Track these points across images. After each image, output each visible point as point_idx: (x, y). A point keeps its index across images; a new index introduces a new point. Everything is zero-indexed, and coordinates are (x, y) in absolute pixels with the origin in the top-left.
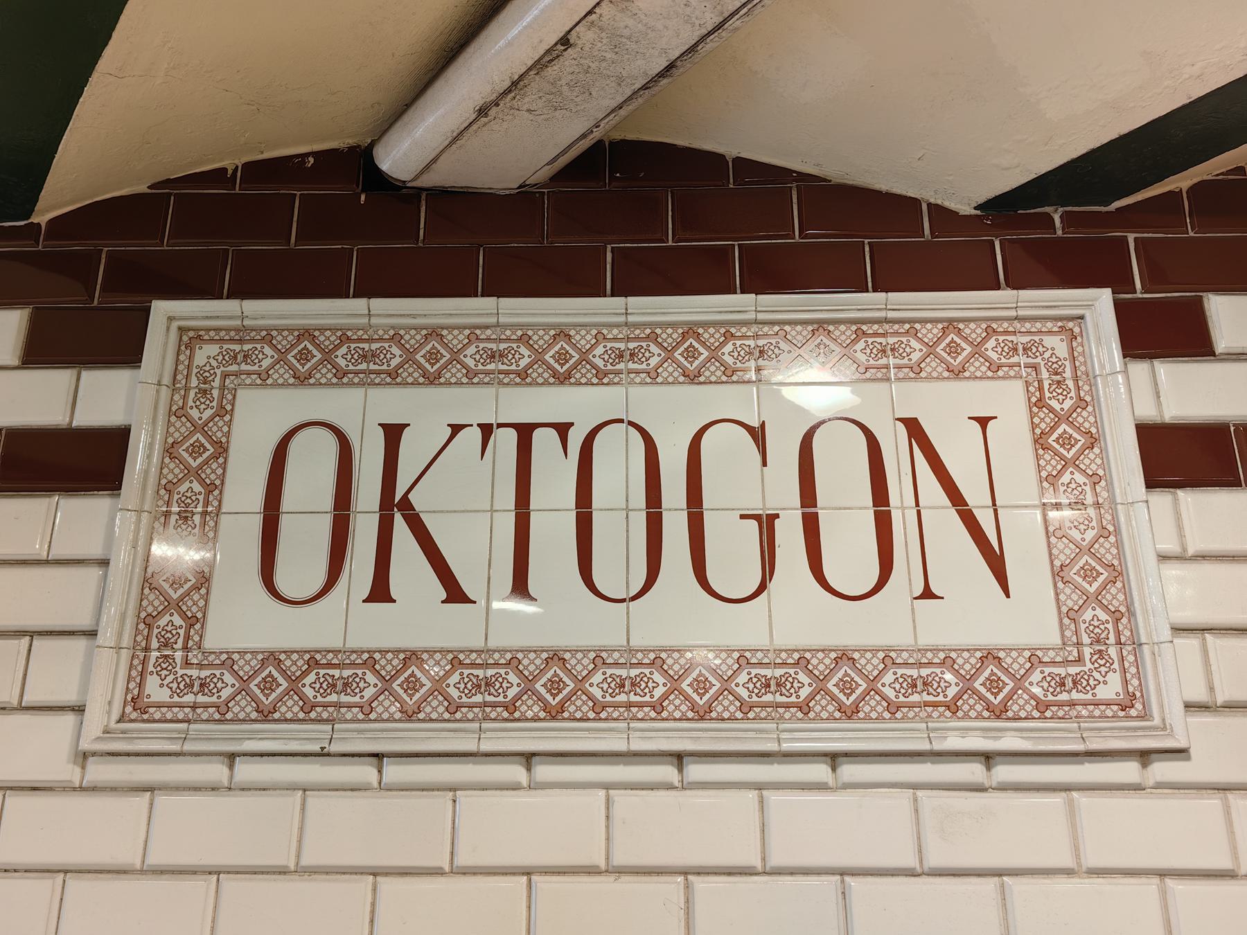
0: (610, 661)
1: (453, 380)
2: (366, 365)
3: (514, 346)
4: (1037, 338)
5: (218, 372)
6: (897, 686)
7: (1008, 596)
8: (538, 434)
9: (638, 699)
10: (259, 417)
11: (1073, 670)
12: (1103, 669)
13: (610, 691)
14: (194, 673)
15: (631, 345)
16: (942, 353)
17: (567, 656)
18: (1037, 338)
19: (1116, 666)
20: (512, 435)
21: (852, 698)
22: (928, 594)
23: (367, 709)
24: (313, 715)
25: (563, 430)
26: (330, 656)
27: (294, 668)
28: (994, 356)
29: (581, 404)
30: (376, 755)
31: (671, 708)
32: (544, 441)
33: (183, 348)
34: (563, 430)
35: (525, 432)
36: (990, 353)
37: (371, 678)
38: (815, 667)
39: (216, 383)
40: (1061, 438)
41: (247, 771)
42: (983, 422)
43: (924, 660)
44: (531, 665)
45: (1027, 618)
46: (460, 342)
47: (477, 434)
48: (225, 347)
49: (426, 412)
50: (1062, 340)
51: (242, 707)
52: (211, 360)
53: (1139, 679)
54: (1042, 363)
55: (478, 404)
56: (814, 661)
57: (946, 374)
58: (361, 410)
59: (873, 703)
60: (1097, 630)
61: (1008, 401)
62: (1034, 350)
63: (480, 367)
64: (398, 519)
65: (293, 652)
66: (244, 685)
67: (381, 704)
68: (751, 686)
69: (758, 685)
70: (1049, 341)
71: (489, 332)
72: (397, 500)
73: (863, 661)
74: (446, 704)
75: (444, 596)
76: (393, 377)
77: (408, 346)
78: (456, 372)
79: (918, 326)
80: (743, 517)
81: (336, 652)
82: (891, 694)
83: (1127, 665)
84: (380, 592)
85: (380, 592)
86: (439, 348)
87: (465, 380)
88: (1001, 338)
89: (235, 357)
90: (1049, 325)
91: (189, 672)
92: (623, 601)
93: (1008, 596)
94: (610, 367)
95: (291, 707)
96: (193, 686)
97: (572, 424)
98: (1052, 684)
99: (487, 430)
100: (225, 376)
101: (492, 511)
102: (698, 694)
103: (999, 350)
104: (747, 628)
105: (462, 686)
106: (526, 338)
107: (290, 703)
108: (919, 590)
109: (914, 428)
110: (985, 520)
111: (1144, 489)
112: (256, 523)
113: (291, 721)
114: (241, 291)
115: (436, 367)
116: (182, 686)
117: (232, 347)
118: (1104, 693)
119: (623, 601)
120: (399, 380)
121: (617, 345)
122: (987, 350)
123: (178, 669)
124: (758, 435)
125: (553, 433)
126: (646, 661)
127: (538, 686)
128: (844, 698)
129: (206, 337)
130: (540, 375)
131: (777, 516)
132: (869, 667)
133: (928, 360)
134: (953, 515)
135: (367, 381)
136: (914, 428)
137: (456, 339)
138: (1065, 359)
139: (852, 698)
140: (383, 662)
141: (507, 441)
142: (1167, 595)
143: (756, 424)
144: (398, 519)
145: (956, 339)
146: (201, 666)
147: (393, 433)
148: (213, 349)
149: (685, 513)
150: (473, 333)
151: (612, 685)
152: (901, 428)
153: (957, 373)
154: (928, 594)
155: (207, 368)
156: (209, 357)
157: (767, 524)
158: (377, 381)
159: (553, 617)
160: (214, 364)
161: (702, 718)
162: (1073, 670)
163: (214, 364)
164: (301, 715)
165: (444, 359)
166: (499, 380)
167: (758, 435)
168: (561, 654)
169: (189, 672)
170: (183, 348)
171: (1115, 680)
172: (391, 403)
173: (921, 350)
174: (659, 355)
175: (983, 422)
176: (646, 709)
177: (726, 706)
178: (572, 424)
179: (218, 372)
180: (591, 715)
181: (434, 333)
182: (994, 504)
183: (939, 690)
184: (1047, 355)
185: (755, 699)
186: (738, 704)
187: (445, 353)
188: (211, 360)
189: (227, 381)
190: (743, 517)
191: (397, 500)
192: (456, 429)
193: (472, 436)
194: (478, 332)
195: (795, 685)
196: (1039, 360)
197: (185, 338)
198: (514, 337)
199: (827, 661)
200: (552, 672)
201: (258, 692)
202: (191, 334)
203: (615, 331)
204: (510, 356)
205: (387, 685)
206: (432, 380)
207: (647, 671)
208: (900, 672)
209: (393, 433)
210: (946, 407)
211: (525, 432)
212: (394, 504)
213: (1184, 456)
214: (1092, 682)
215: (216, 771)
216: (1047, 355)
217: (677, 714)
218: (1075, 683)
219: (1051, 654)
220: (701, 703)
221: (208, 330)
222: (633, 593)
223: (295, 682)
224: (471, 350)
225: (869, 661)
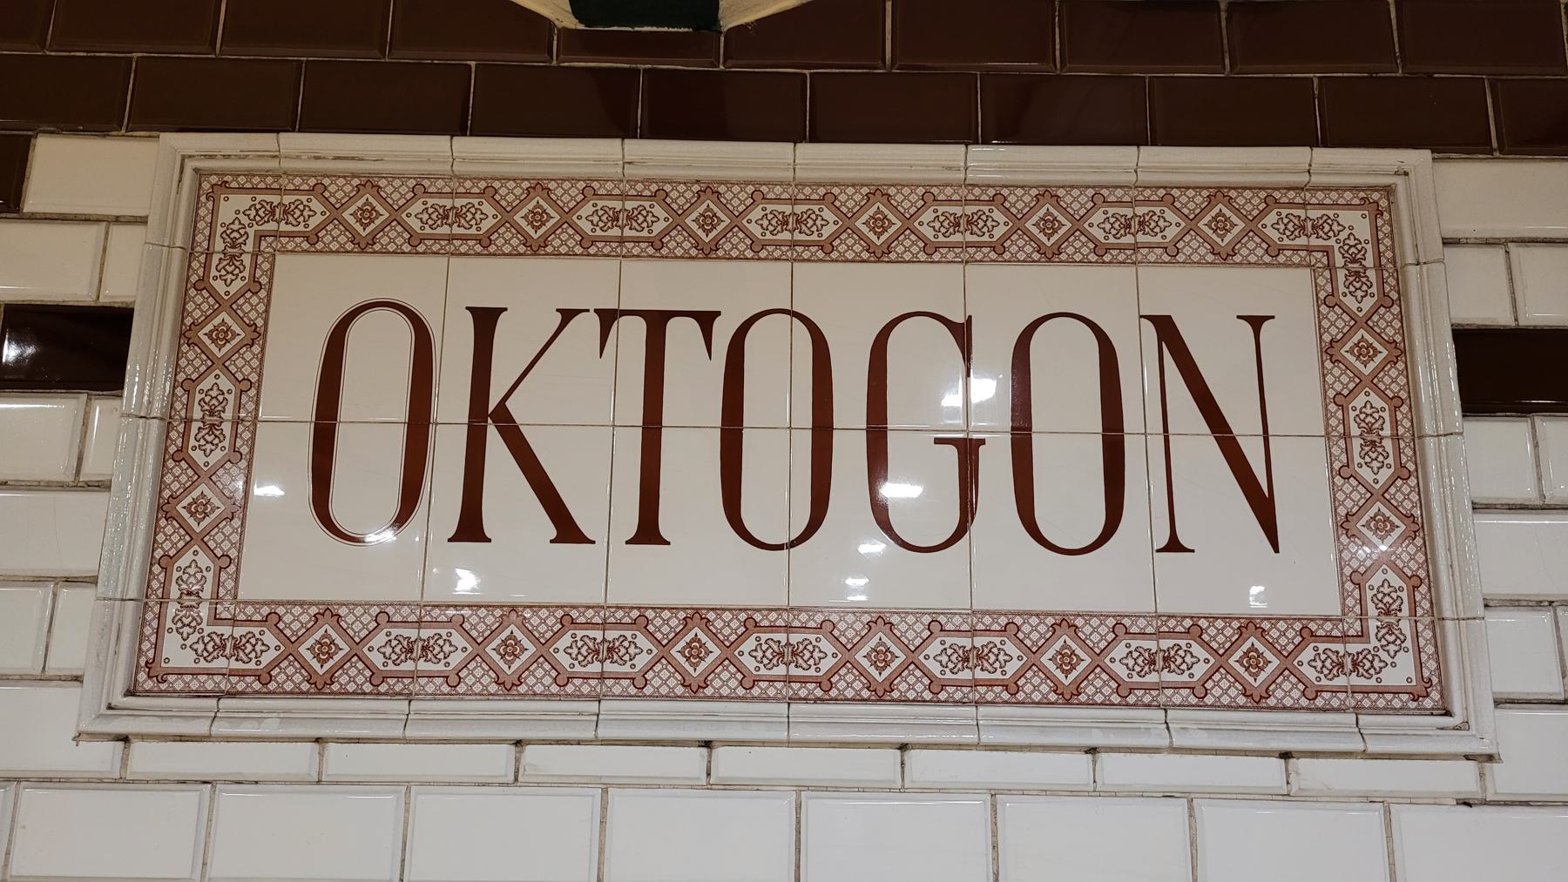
0: (397, 618)
1: (1078, 257)
2: (454, 229)
3: (647, 204)
4: (1331, 213)
5: (251, 231)
6: (1131, 662)
7: (1276, 550)
8: (673, 325)
9: (986, 675)
10: (308, 293)
11: (1354, 648)
12: (1392, 648)
13: (951, 665)
14: (226, 630)
15: (1140, 211)
16: (1206, 229)
17: (343, 611)
18: (1331, 213)
19: (1408, 644)
20: (640, 325)
21: (886, 673)
22: (1174, 545)
23: (453, 680)
24: (756, 691)
25: (706, 320)
26: (773, 615)
27: (543, 628)
28: (1274, 235)
29: (733, 288)
30: (317, 740)
31: (842, 685)
32: (681, 333)
33: (203, 199)
34: (706, 320)
35: (657, 322)
36: (1269, 231)
37: (642, 641)
38: (1027, 636)
39: (249, 247)
40: (1360, 344)
41: (340, 759)
42: (1256, 322)
43: (980, 627)
44: (294, 621)
45: (1292, 580)
46: (913, 204)
47: (594, 322)
48: (260, 198)
49: (529, 290)
50: (1364, 216)
51: (478, 678)
52: (241, 216)
53: (1438, 661)
54: (1336, 246)
55: (593, 282)
56: (1027, 628)
57: (1210, 258)
58: (445, 289)
59: (1098, 683)
60: (1387, 599)
61: (1288, 294)
62: (1327, 228)
63: (769, 236)
64: (493, 436)
65: (541, 607)
66: (356, 650)
67: (657, 675)
68: (944, 659)
69: (954, 658)
70: (1347, 217)
71: (440, 183)
72: (491, 409)
73: (1088, 629)
74: (739, 676)
75: (553, 533)
76: (485, 244)
77: (504, 203)
78: (395, 236)
79: (1176, 193)
80: (938, 441)
81: (596, 608)
82: (935, 668)
83: (1422, 642)
84: (470, 528)
85: (470, 528)
86: (545, 206)
87: (578, 250)
88: (1284, 212)
89: (273, 212)
90: (1348, 195)
91: (219, 629)
92: (779, 547)
93: (1276, 550)
94: (941, 239)
95: (540, 678)
96: (224, 647)
97: (718, 314)
98: (1140, 661)
99: (608, 318)
100: (260, 237)
101: (1145, 434)
102: (1063, 671)
103: (1282, 227)
104: (938, 585)
105: (760, 654)
106: (491, 191)
107: (539, 673)
108: (1163, 539)
109: (1166, 329)
110: (1253, 451)
111: (1458, 413)
112: (306, 435)
113: (729, 698)
114: (661, 129)
115: (541, 232)
116: (210, 647)
117: (269, 198)
118: (1391, 678)
119: (779, 547)
120: (664, 251)
121: (780, 208)
122: (1265, 226)
123: (204, 625)
124: (962, 333)
125: (693, 324)
126: (995, 627)
127: (303, 650)
128: (875, 673)
129: (234, 185)
130: (1021, 249)
131: (983, 442)
132: (1095, 637)
133: (1187, 238)
134: (1210, 446)
135: (450, 247)
136: (1166, 329)
137: (396, 192)
138: (1367, 242)
139: (886, 673)
140: (658, 622)
141: (632, 332)
142: (1499, 556)
143: (960, 319)
144: (493, 436)
145: (1225, 210)
146: (234, 621)
147: (485, 320)
148: (243, 201)
149: (1100, 438)
150: (1099, 195)
151: (623, 651)
152: (1149, 327)
153: (1225, 257)
154: (1174, 545)
155: (236, 227)
156: (237, 212)
157: (968, 451)
158: (434, 249)
159: (702, 565)
160: (245, 220)
161: (880, 699)
162: (1354, 648)
163: (245, 220)
164: (741, 692)
165: (381, 219)
166: (620, 249)
167: (962, 333)
168: (887, 617)
169: (219, 629)
170: (203, 199)
171: (1406, 662)
172: (484, 281)
173: (1178, 225)
174: (921, 224)
175: (1256, 322)
176: (997, 689)
177: (912, 685)
178: (718, 314)
179: (251, 231)
180: (927, 695)
181: (708, 189)
182: (1166, 429)
183: (811, 662)
184: (1343, 236)
185: (949, 675)
186: (926, 681)
187: (553, 213)
188: (241, 216)
189: (264, 244)
190: (938, 441)
191: (491, 409)
192: (568, 315)
193: (588, 325)
194: (1105, 192)
195: (1001, 657)
196: (1332, 242)
197: (206, 186)
198: (647, 193)
199: (1042, 629)
200: (322, 632)
201: (497, 658)
202: (214, 180)
203: (778, 190)
204: (810, 222)
205: (1098, 660)
206: (535, 249)
207: (812, 637)
208: (1135, 644)
209: (485, 320)
210: (1208, 303)
211: (657, 322)
212: (488, 415)
213: (1512, 371)
214: (1377, 664)
215: (300, 758)
216: (1343, 236)
217: (850, 693)
218: (1355, 664)
219: (957, 620)
220: (880, 679)
221: (236, 175)
222: (795, 535)
223: (729, 648)
224: (417, 207)
225: (1095, 630)
